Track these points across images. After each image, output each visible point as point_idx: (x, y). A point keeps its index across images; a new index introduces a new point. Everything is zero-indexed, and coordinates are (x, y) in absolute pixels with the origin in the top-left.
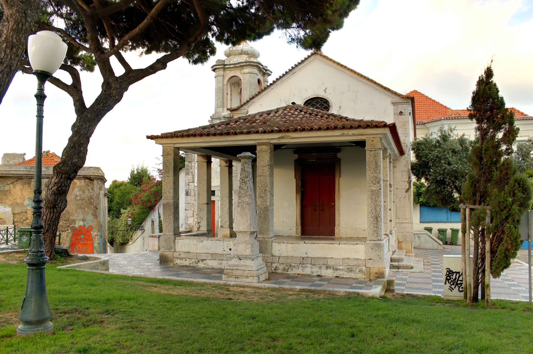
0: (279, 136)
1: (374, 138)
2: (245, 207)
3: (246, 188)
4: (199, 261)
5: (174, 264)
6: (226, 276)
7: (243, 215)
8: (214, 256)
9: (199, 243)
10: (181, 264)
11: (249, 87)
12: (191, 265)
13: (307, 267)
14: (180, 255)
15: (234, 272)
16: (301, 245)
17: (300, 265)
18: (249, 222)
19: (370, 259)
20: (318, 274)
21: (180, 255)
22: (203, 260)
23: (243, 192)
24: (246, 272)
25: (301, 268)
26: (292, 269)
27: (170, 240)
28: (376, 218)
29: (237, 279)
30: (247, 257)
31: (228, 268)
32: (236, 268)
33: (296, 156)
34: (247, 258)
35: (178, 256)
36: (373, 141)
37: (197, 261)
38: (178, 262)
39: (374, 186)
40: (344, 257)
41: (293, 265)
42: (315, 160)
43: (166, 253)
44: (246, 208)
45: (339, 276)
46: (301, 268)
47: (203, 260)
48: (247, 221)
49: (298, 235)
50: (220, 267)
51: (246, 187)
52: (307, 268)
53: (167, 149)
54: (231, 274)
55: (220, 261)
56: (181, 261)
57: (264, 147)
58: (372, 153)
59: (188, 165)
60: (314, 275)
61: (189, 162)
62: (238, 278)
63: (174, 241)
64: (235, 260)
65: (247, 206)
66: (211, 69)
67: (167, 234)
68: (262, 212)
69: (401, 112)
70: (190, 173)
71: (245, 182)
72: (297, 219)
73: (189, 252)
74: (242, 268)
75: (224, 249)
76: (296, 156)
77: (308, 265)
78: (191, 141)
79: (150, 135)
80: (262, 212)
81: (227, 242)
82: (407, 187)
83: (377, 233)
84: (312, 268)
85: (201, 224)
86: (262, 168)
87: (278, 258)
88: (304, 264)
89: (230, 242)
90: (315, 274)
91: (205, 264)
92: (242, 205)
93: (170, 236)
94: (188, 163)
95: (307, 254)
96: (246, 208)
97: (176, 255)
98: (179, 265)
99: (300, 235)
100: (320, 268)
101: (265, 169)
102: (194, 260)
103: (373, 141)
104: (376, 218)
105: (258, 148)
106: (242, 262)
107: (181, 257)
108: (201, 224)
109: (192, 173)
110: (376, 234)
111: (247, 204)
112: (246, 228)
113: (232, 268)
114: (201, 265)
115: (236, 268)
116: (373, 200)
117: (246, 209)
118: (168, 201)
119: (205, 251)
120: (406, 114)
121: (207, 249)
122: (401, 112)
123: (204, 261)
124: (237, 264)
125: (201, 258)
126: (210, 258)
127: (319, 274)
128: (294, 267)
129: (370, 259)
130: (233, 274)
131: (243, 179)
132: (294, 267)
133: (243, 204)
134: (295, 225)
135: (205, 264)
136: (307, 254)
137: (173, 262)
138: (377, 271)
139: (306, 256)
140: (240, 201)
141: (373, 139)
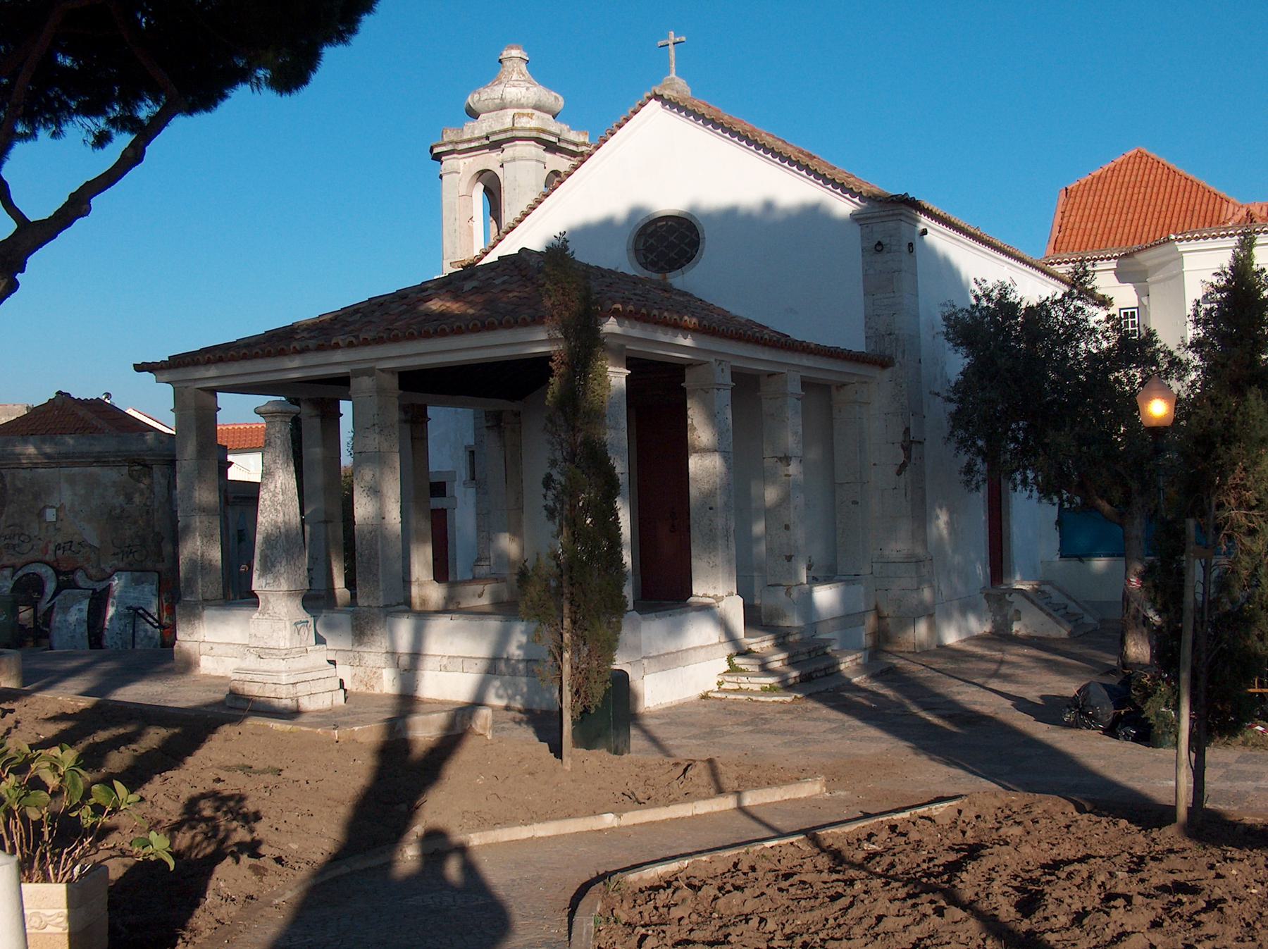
14: (212, 648)
21: (212, 648)
69: (879, 243)
82: (901, 459)
106: (265, 664)
115: (250, 676)
122: (879, 243)
124: (253, 668)
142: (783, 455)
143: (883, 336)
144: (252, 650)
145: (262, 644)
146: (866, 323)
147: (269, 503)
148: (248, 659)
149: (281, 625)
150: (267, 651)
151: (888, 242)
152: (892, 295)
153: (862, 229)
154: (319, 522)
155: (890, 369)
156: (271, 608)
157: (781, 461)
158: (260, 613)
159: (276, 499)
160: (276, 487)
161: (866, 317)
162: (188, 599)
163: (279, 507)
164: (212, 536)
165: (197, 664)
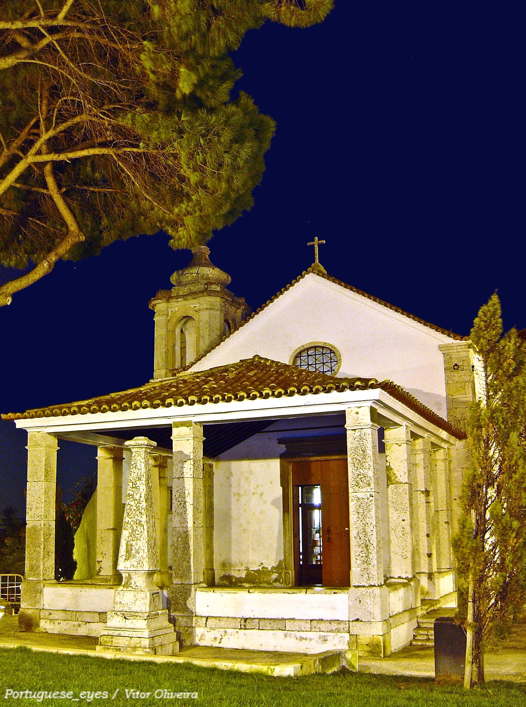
1: (358, 408)
2: (135, 528)
11: (208, 332)
14: (50, 614)
15: (114, 640)
19: (357, 620)
21: (50, 614)
28: (367, 546)
31: (106, 633)
32: (118, 632)
35: (47, 616)
39: (360, 490)
40: (311, 619)
51: (139, 495)
57: (184, 430)
68: (180, 539)
69: (456, 365)
74: (127, 633)
80: (180, 539)
83: (368, 574)
87: (205, 619)
103: (357, 413)
105: (175, 431)
106: (129, 624)
107: (51, 617)
113: (111, 633)
115: (118, 632)
120: (465, 368)
122: (456, 365)
124: (121, 626)
129: (357, 620)
138: (368, 641)
141: (357, 410)
142: (424, 490)
143: (459, 421)
144: (118, 613)
145: (126, 609)
146: (448, 413)
147: (135, 508)
148: (114, 620)
149: (142, 595)
150: (132, 614)
151: (461, 364)
152: (465, 396)
153: (444, 356)
154: (110, 529)
155: (464, 441)
156: (133, 583)
157: (423, 493)
158: (124, 586)
159: (141, 505)
160: (140, 497)
161: (448, 409)
162: (31, 578)
163: (143, 511)
164: (50, 535)
165: (38, 625)
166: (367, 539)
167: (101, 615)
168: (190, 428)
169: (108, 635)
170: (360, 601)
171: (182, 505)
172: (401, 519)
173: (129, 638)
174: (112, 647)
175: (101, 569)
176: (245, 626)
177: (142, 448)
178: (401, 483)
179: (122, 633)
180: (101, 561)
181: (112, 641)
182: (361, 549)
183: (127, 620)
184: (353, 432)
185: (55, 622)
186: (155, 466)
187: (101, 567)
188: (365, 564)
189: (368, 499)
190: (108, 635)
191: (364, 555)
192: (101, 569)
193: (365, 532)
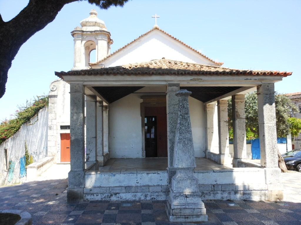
0: (191, 79)
2: (186, 143)
3: (187, 124)
4: (111, 195)
5: (84, 201)
6: (175, 217)
7: (185, 151)
8: (128, 188)
9: (110, 177)
10: (92, 200)
12: (104, 199)
13: (217, 193)
16: (211, 173)
17: (212, 192)
18: (192, 158)
20: (227, 199)
22: (116, 194)
23: (183, 128)
24: (196, 210)
25: (212, 195)
26: (204, 196)
27: (80, 176)
28: (273, 149)
29: (186, 219)
30: (195, 194)
32: (184, 207)
33: (142, 101)
34: (194, 195)
36: (268, 86)
37: (109, 195)
38: (89, 197)
41: (205, 192)
42: (155, 103)
43: (76, 190)
44: (188, 144)
45: (246, 199)
46: (212, 195)
47: (116, 194)
48: (190, 157)
49: (144, 158)
50: (134, 199)
51: (187, 123)
52: (217, 195)
53: (75, 87)
54: (180, 214)
55: (135, 194)
56: (92, 197)
58: (268, 96)
59: (51, 106)
60: (224, 200)
61: (52, 103)
62: (188, 218)
63: (84, 177)
64: (181, 198)
65: (189, 142)
66: (71, 34)
67: (75, 170)
70: (53, 112)
71: (185, 119)
72: (142, 146)
73: (100, 187)
74: (191, 207)
75: (137, 182)
76: (142, 101)
77: (219, 192)
78: (104, 80)
79: (59, 71)
81: (140, 175)
84: (222, 194)
85: (90, 156)
86: (173, 106)
88: (215, 191)
89: (143, 174)
90: (225, 199)
91: (118, 197)
92: (184, 141)
93: (79, 172)
94: (51, 104)
95: (216, 181)
96: (188, 144)
97: (85, 191)
98: (90, 200)
99: (145, 157)
100: (229, 193)
101: (176, 107)
102: (107, 195)
104: (273, 149)
108: (90, 156)
109: (55, 112)
110: (273, 163)
111: (189, 140)
112: (189, 164)
114: (114, 198)
116: (270, 135)
117: (188, 145)
118: (77, 137)
119: (117, 185)
121: (120, 182)
123: (117, 195)
124: (184, 203)
125: (114, 192)
126: (124, 191)
127: (229, 198)
128: (206, 194)
130: (182, 214)
131: (183, 115)
132: (206, 194)
133: (184, 140)
134: (141, 150)
135: (118, 197)
136: (216, 181)
137: (83, 198)
139: (215, 183)
140: (181, 137)
141: (268, 85)
154: (93, 138)
166: (273, 145)
167: (127, 188)
168: (178, 87)
169: (177, 209)
170: (272, 175)
171: (174, 127)
172: (242, 134)
173: (193, 210)
174: (182, 216)
175: (89, 158)
176: (214, 189)
177: (272, 92)
178: (242, 118)
179: (187, 207)
180: (89, 154)
181: (181, 213)
182: (271, 150)
183: (187, 198)
184: (266, 95)
185: (94, 195)
186: (100, 106)
187: (89, 157)
188: (273, 157)
189: (273, 127)
190: (177, 209)
191: (272, 153)
192: (89, 158)
193: (272, 142)
